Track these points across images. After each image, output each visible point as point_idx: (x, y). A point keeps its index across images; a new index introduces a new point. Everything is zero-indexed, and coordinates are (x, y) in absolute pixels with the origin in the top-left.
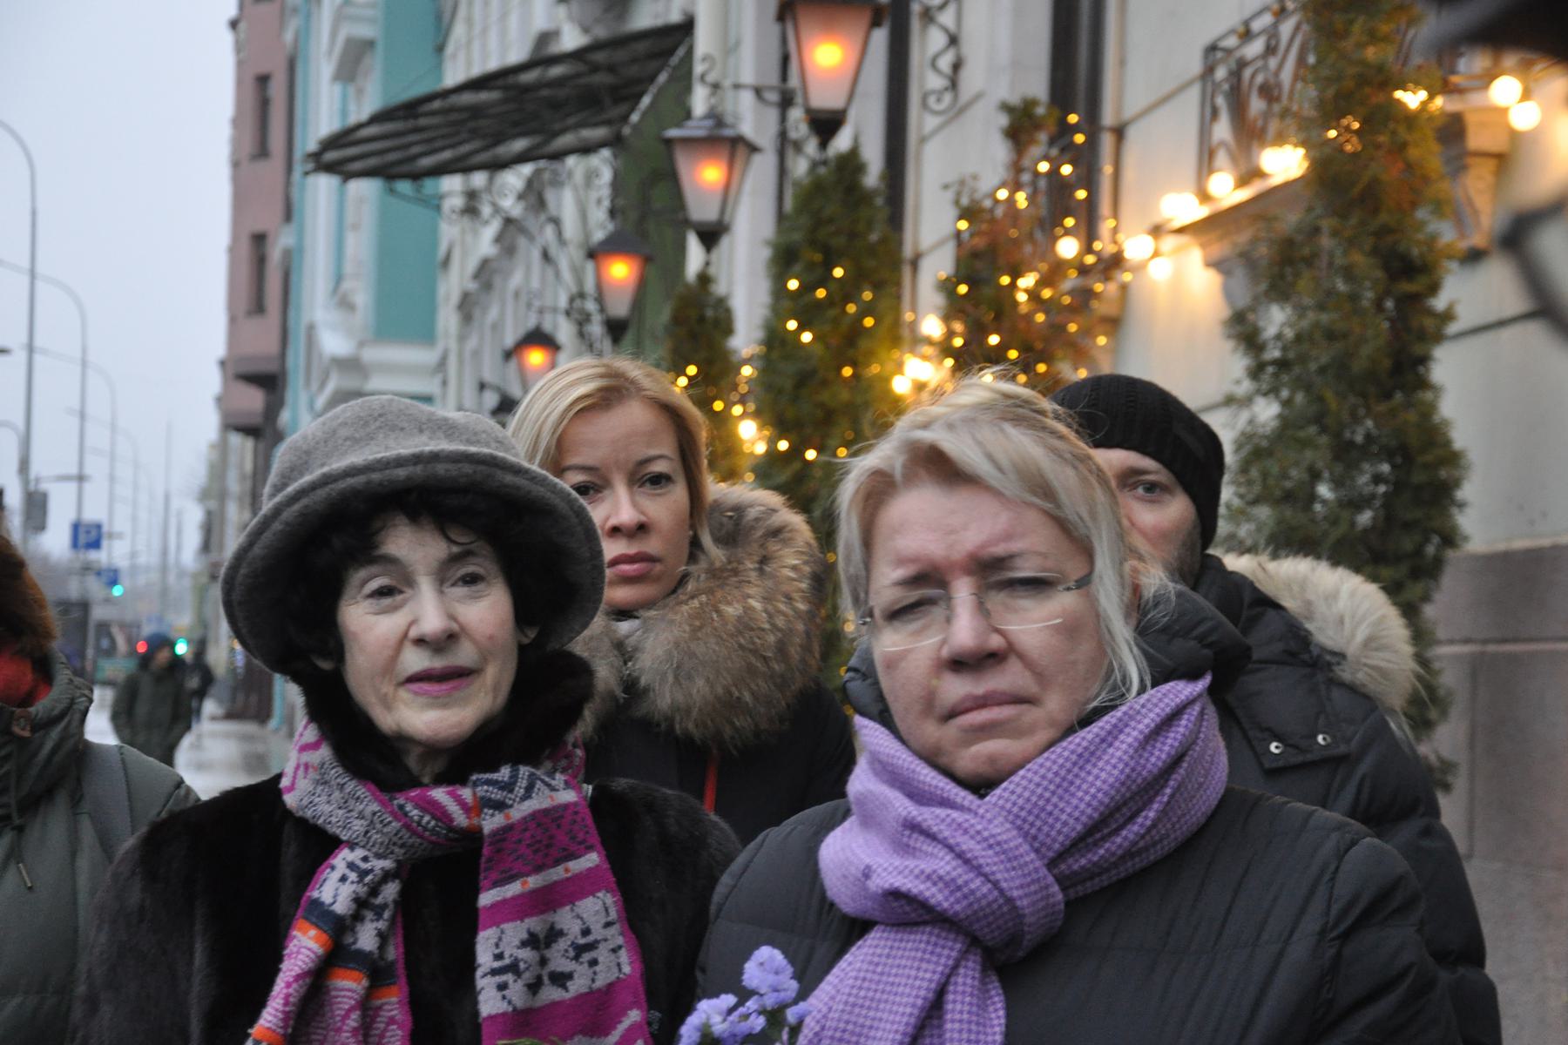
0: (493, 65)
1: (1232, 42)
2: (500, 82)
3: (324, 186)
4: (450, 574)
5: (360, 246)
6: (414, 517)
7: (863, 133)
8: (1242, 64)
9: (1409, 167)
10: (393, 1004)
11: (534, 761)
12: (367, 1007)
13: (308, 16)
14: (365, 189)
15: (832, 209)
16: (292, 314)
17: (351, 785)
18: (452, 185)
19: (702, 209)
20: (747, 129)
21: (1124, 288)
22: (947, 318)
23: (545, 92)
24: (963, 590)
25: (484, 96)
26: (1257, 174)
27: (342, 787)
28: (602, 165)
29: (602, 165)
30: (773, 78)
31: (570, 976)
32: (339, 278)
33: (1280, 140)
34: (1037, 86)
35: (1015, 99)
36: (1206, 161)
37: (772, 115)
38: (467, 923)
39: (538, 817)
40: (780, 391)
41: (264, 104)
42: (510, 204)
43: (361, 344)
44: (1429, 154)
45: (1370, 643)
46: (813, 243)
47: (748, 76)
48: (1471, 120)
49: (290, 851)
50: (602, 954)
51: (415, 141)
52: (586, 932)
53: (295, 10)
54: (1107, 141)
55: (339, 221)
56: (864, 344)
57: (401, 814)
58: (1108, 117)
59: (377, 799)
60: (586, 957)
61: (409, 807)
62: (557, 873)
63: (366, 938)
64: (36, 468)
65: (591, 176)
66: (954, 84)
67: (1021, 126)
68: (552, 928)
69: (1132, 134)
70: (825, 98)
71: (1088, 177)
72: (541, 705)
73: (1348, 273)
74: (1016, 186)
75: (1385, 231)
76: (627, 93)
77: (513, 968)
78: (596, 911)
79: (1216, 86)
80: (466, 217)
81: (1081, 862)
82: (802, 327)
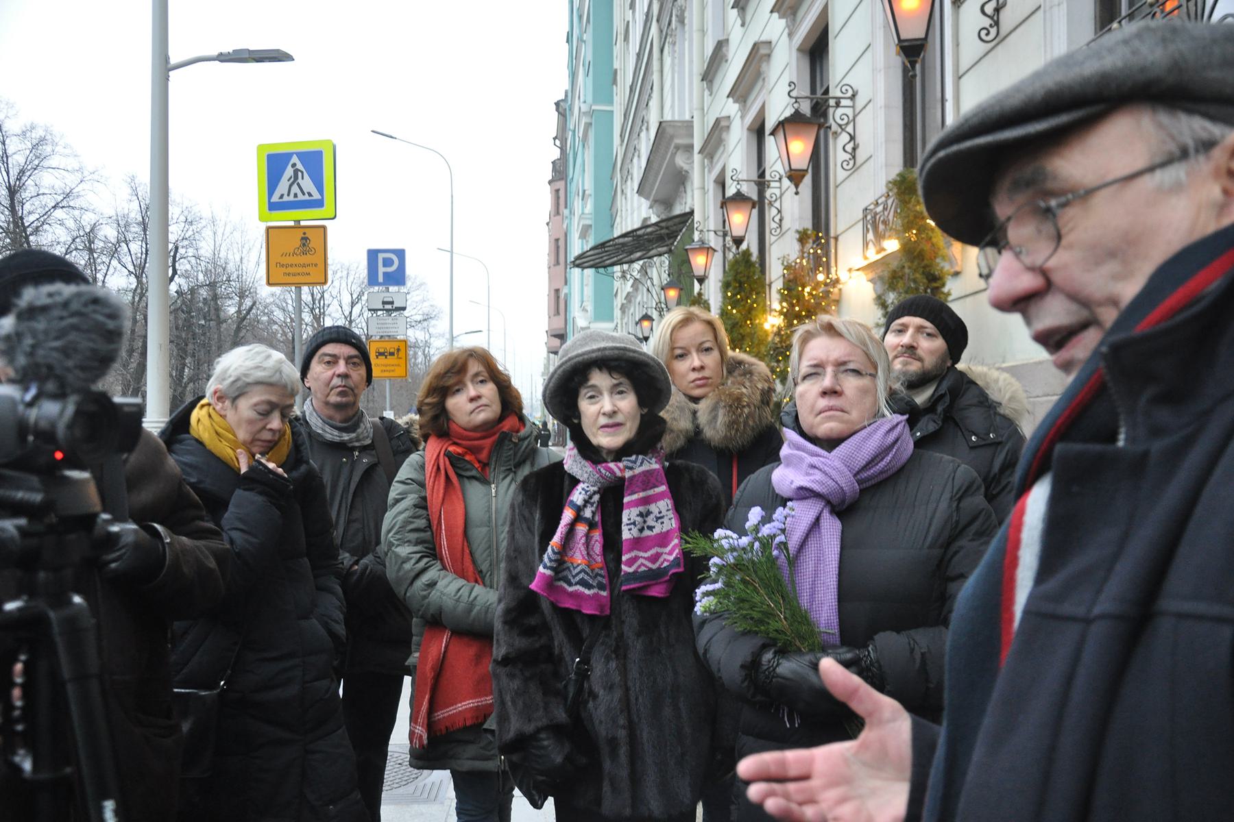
0: (629, 229)
3: (576, 272)
4: (616, 390)
5: (589, 291)
6: (600, 369)
7: (751, 243)
8: (876, 214)
9: (933, 245)
10: (597, 535)
14: (590, 272)
15: (741, 269)
17: (584, 462)
18: (617, 268)
19: (698, 271)
20: (712, 244)
22: (781, 303)
24: (830, 370)
26: (884, 250)
28: (665, 259)
29: (665, 259)
30: (721, 228)
33: (890, 237)
34: (808, 224)
35: (801, 229)
36: (866, 244)
37: (721, 239)
38: (620, 508)
41: (558, 248)
45: (1012, 399)
46: (735, 280)
47: (712, 228)
49: (567, 482)
50: (665, 520)
51: (609, 254)
54: (832, 242)
55: (582, 282)
56: (754, 313)
58: (832, 234)
62: (651, 492)
63: (588, 513)
67: (803, 238)
69: (840, 238)
70: (738, 232)
71: (827, 255)
72: (648, 436)
73: (915, 281)
74: (803, 258)
76: (673, 235)
77: (634, 523)
78: (664, 506)
80: (622, 281)
81: (865, 475)
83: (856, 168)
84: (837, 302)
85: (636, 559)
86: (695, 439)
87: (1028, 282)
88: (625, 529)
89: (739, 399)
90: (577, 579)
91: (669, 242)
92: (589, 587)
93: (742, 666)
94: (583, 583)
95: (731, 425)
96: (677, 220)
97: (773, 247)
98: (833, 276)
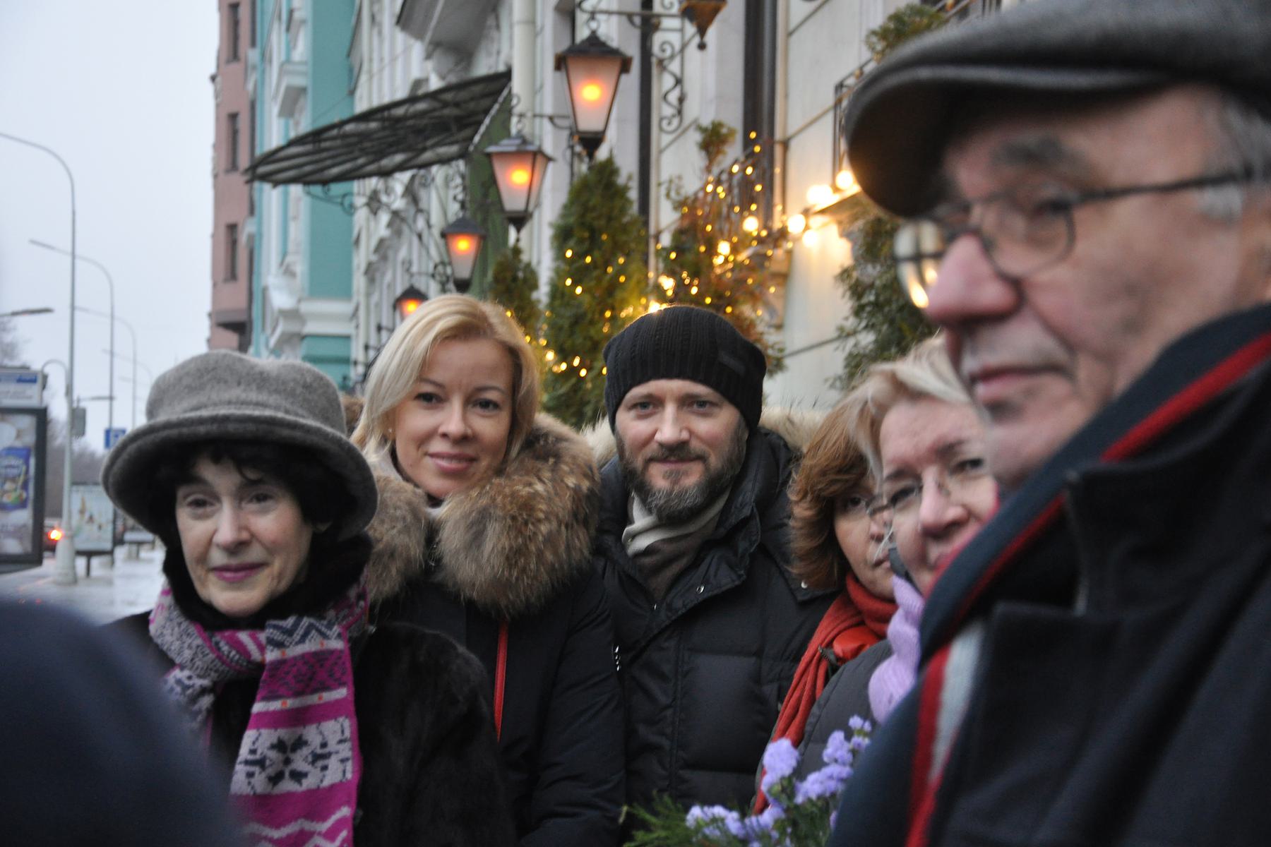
2: (379, 116)
4: (251, 493)
5: (299, 231)
13: (263, 72)
14: (296, 190)
15: (595, 200)
16: (255, 277)
17: (185, 625)
20: (548, 148)
21: (790, 253)
23: (410, 122)
24: (930, 477)
25: (362, 127)
27: (180, 624)
31: (305, 775)
32: (284, 254)
39: (305, 657)
40: (561, 329)
41: (234, 134)
42: (399, 203)
43: (299, 301)
46: (583, 225)
47: (548, 109)
50: (333, 762)
51: (336, 154)
52: (324, 745)
53: (254, 68)
54: (778, 150)
55: (284, 211)
56: (619, 295)
58: (778, 135)
59: (200, 635)
60: (320, 763)
61: (222, 644)
62: (314, 699)
64: (77, 393)
65: (447, 181)
66: (680, 112)
68: (300, 738)
69: (794, 145)
70: (589, 123)
71: (766, 177)
72: (323, 579)
76: (469, 122)
77: (261, 763)
78: (337, 734)
80: (374, 207)
82: (575, 284)
84: (783, 278)
86: (426, 583)
88: (240, 770)
89: (527, 505)
91: (466, 133)
95: (514, 556)
96: (477, 89)
98: (777, 225)
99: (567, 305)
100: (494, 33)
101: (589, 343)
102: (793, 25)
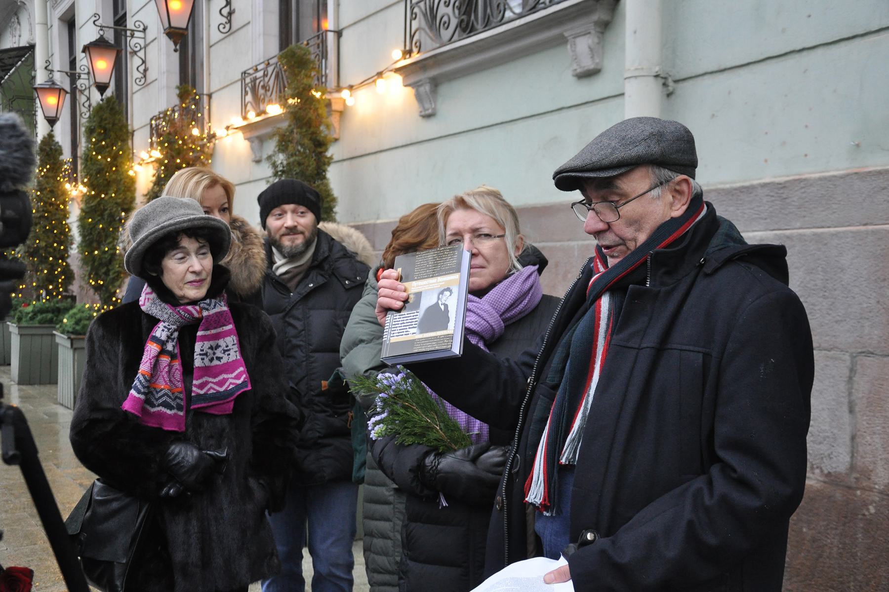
1: (251, 71)
8: (256, 79)
9: (318, 115)
10: (177, 364)
11: (215, 298)
12: (170, 366)
17: (163, 305)
24: (467, 237)
26: (264, 112)
36: (244, 106)
38: (193, 340)
44: (323, 111)
48: (333, 101)
50: (232, 352)
52: (227, 346)
54: (205, 98)
56: (119, 160)
57: (179, 313)
62: (220, 330)
69: (214, 96)
70: (102, 79)
72: (220, 281)
73: (302, 145)
75: (313, 133)
77: (206, 354)
78: (231, 341)
79: (246, 85)
81: (508, 315)
82: (97, 154)
83: (230, 32)
85: (207, 383)
87: (601, 226)
90: (160, 401)
92: (171, 408)
93: (410, 470)
94: (166, 405)
97: (135, 96)
99: (94, 164)
100: (16, 25)
101: (105, 182)
102: (212, 43)
